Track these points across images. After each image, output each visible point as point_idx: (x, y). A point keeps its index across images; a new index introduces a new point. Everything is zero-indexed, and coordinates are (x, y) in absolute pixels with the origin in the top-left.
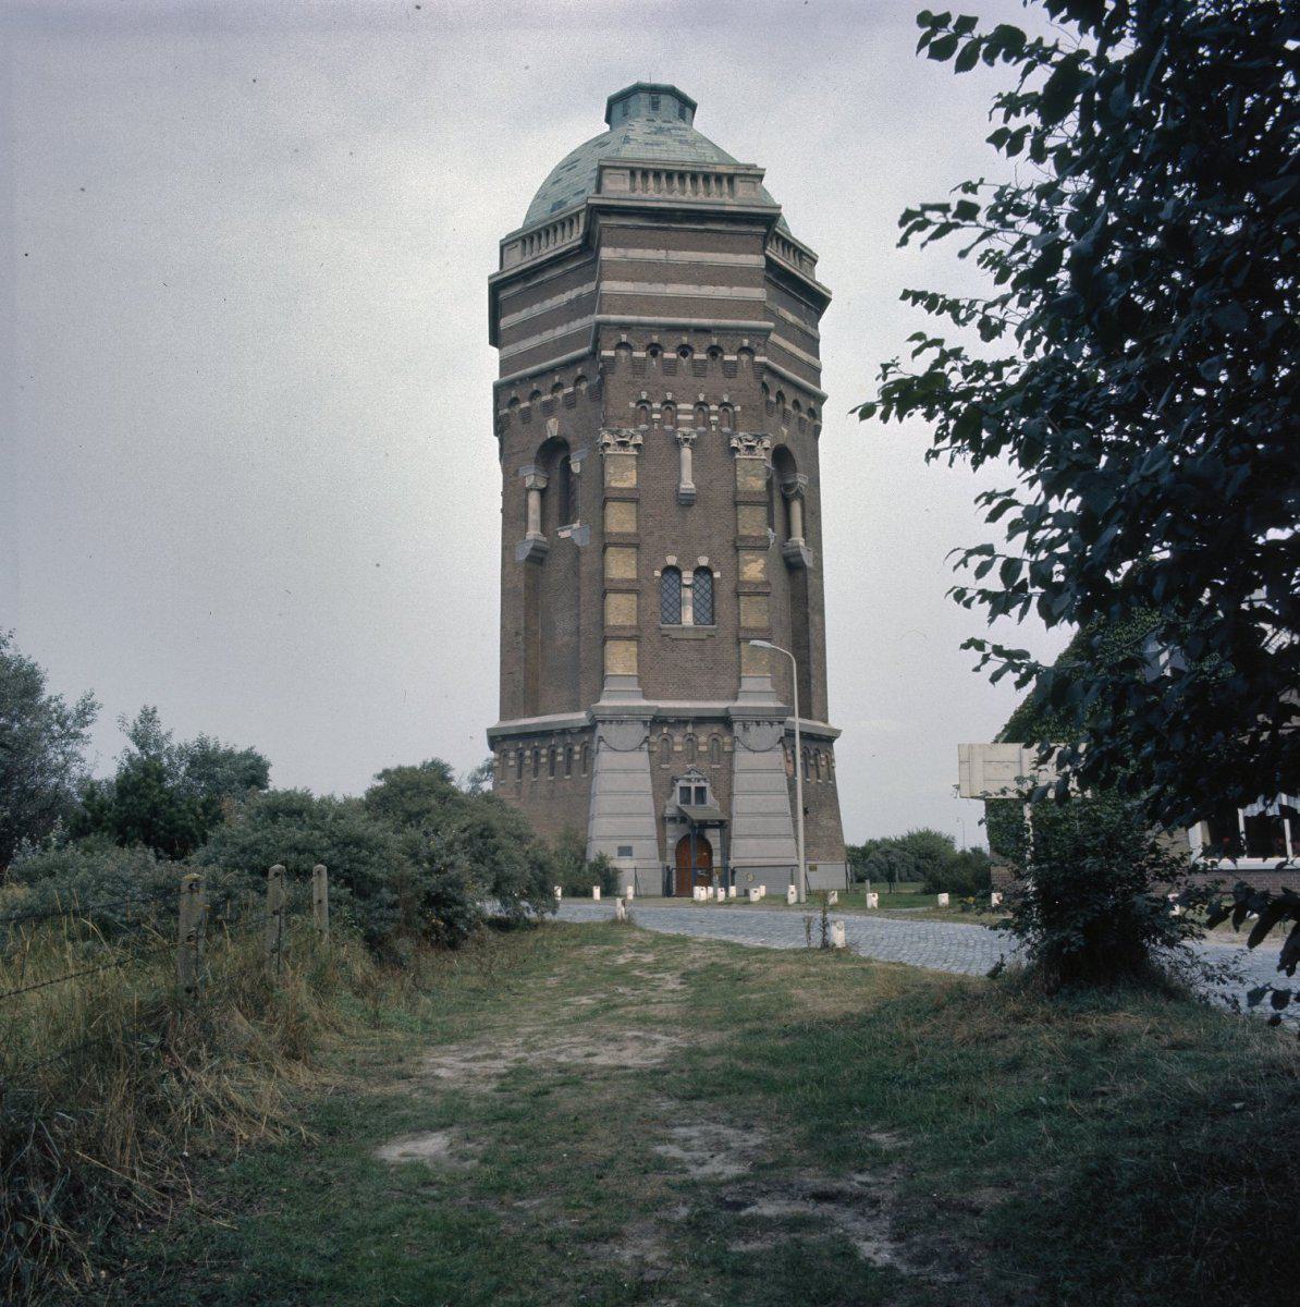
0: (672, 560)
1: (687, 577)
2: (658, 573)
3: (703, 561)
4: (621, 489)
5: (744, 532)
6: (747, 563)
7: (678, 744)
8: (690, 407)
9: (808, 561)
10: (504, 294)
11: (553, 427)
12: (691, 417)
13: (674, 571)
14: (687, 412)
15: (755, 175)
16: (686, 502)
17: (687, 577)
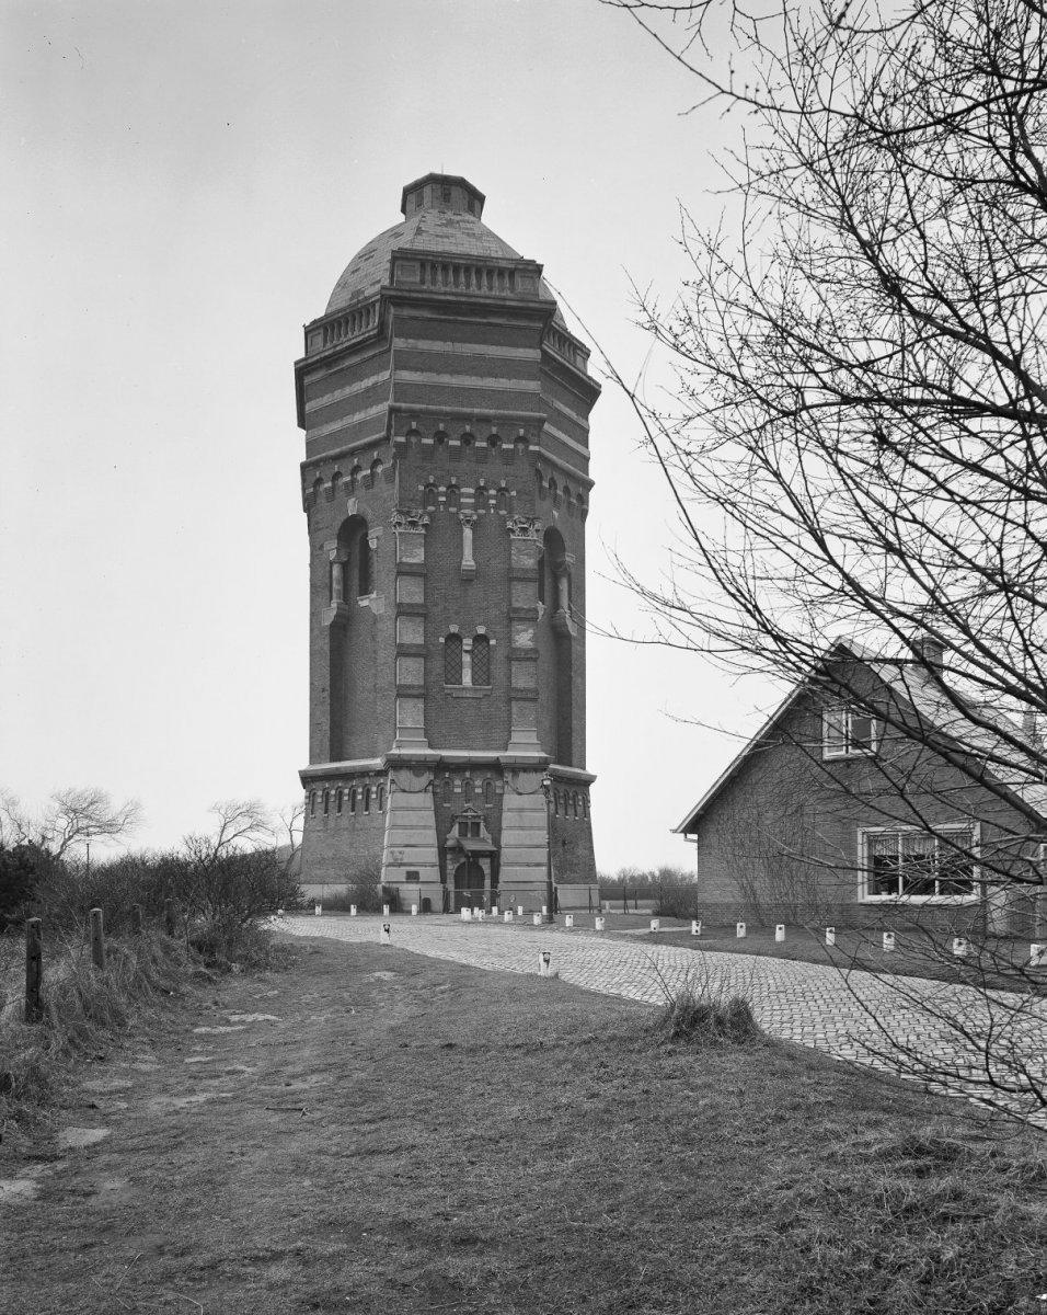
0: (454, 629)
1: (467, 643)
2: (442, 640)
3: (481, 630)
4: (411, 565)
5: (516, 605)
6: (518, 632)
7: (458, 786)
8: (472, 491)
9: (572, 630)
10: (307, 380)
11: (352, 508)
12: (472, 501)
13: (454, 639)
14: (469, 496)
15: (537, 269)
16: (468, 579)
17: (467, 643)
